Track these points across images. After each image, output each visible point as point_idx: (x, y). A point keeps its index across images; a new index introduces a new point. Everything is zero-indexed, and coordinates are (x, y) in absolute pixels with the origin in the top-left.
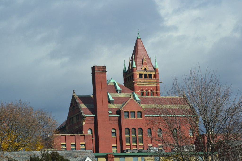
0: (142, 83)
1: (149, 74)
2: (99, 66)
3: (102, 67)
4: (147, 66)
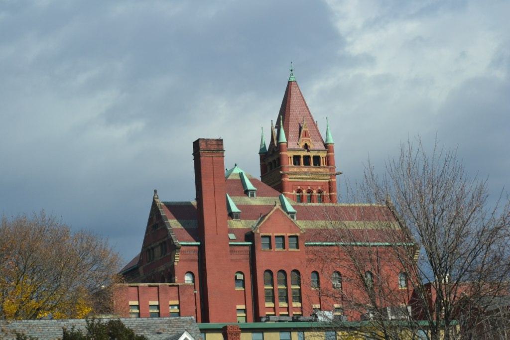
0: (300, 175)
1: (315, 157)
2: (208, 139)
3: (214, 142)
4: (308, 139)
